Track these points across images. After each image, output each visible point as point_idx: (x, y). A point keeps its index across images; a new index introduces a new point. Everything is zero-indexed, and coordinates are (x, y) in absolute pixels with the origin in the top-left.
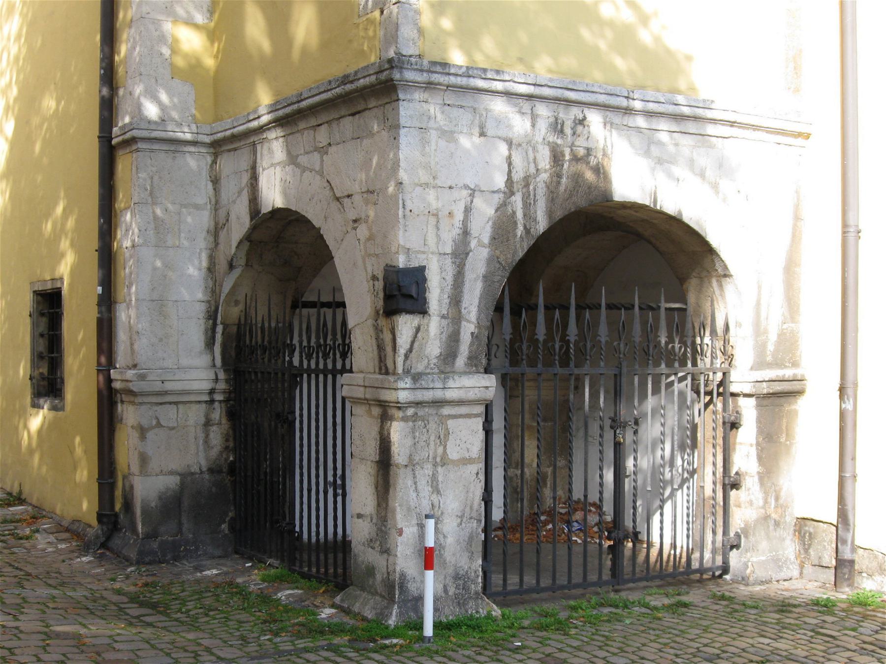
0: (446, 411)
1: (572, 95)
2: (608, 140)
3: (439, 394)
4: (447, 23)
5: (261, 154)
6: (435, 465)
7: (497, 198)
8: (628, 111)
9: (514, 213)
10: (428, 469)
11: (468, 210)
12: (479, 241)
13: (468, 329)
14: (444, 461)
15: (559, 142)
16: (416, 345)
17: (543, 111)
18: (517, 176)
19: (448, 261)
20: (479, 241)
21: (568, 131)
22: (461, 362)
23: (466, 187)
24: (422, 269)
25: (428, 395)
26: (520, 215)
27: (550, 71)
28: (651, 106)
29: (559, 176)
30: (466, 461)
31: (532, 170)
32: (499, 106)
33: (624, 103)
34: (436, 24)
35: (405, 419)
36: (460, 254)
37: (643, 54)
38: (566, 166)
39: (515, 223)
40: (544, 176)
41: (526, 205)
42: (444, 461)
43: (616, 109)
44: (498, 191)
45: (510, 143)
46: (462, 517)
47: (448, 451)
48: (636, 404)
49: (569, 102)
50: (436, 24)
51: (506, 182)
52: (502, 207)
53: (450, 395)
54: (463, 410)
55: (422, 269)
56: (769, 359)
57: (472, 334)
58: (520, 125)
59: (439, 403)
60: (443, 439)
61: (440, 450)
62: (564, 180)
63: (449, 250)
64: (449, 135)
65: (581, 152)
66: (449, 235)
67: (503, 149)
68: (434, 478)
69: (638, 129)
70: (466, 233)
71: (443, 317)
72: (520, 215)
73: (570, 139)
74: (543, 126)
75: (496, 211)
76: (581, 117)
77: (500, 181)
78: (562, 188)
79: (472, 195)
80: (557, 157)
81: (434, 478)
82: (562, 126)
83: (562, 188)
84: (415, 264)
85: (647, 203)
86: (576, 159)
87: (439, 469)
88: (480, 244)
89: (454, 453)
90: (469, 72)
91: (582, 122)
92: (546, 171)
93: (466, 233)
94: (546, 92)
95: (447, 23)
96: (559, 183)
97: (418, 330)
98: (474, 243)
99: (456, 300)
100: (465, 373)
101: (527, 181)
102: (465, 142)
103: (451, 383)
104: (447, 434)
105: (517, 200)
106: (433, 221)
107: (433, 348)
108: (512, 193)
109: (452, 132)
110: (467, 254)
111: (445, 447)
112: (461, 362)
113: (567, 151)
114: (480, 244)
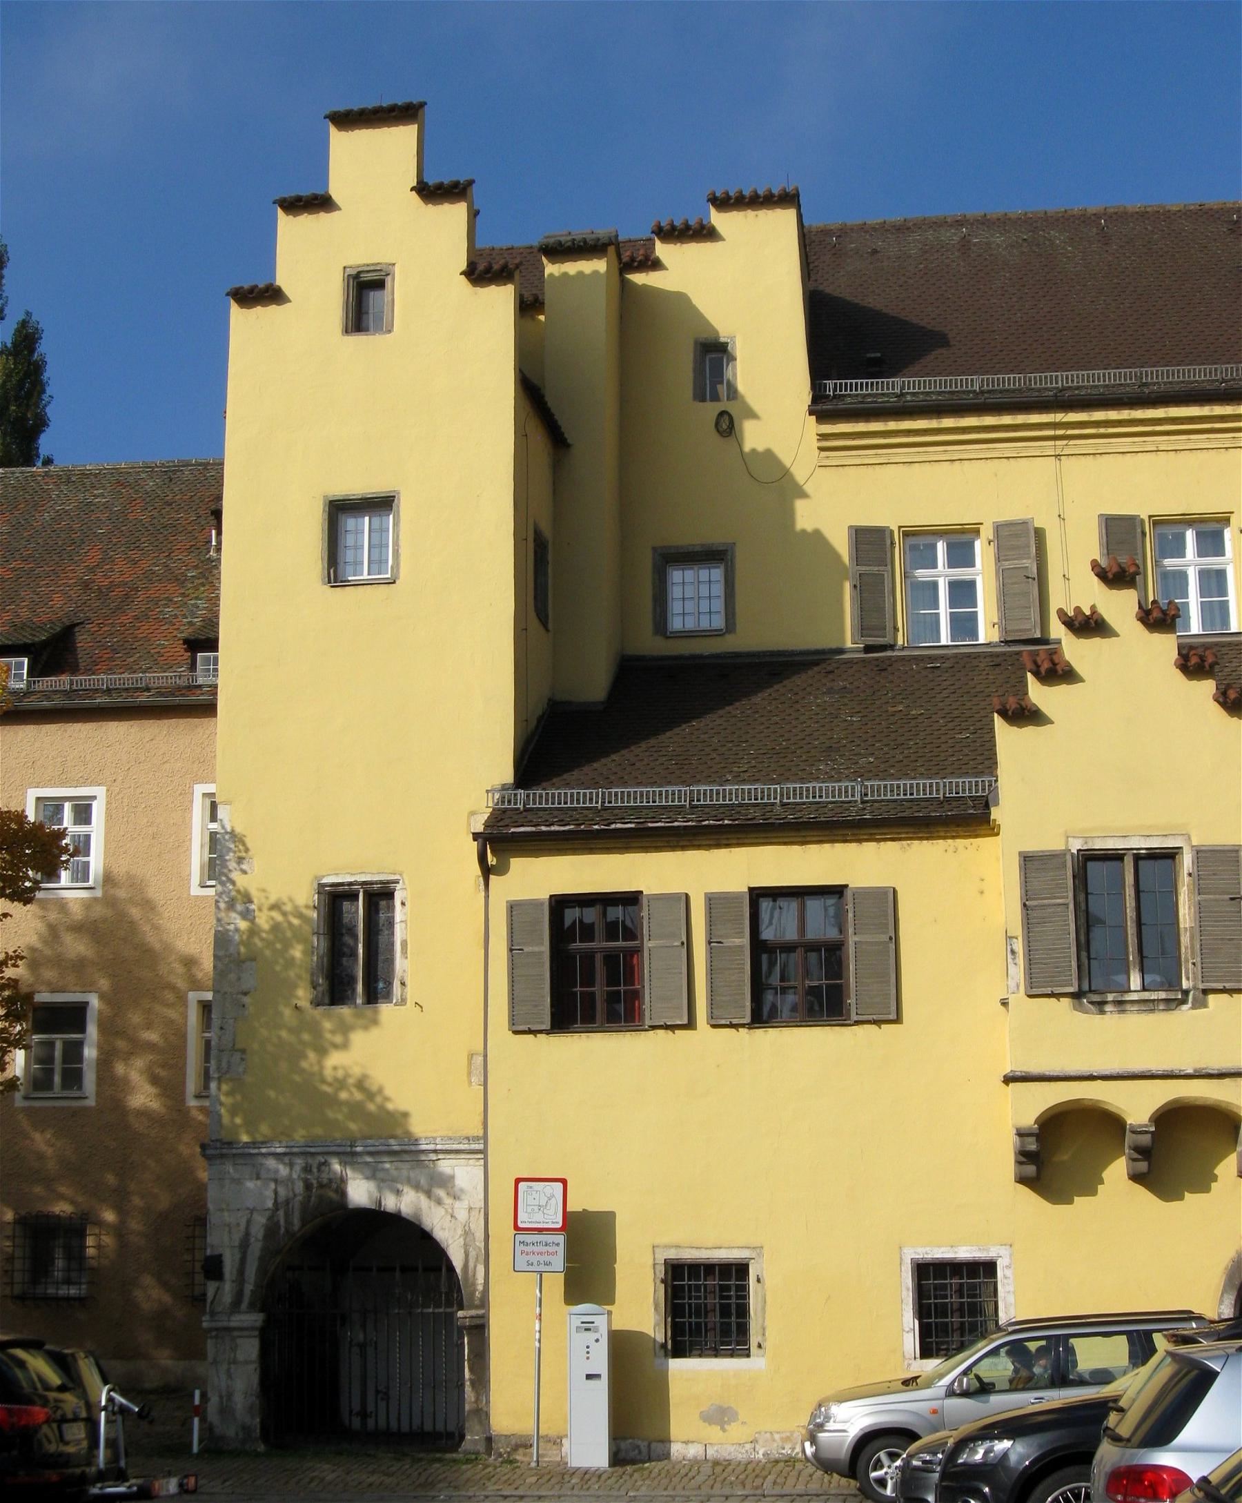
0: (236, 1333)
1: (312, 1150)
2: (344, 1172)
3: (225, 1324)
4: (238, 1121)
5: (469, 1159)
6: (229, 1364)
7: (268, 1214)
8: (354, 1154)
9: (278, 1221)
10: (225, 1366)
11: (249, 1222)
12: (256, 1238)
13: (249, 1288)
14: (235, 1362)
15: (309, 1177)
16: (217, 1297)
17: (299, 1162)
18: (280, 1200)
19: (236, 1251)
20: (256, 1238)
21: (315, 1170)
22: (244, 1306)
23: (248, 1209)
24: (220, 1256)
25: (220, 1324)
26: (282, 1222)
27: (304, 1137)
28: (371, 1149)
29: (310, 1197)
30: (247, 1362)
31: (291, 1195)
32: (271, 1163)
33: (349, 1149)
34: (232, 1122)
35: (211, 1338)
36: (244, 1245)
37: (367, 1117)
38: (314, 1190)
39: (280, 1227)
40: (300, 1198)
41: (287, 1215)
42: (235, 1362)
43: (344, 1153)
44: (269, 1209)
45: (276, 1181)
46: (246, 1393)
47: (238, 1356)
48: (78, 1471)
49: (313, 1154)
50: (232, 1122)
51: (273, 1204)
52: (270, 1218)
53: (232, 1324)
54: (246, 1333)
55: (220, 1256)
56: (477, 1302)
57: (252, 1291)
58: (283, 1171)
59: (228, 1329)
60: (234, 1349)
61: (232, 1355)
62: (313, 1198)
63: (237, 1244)
64: (238, 1182)
65: (325, 1181)
66: (237, 1237)
67: (272, 1186)
68: (228, 1371)
69: (367, 1163)
70: (247, 1234)
71: (233, 1281)
72: (282, 1222)
73: (316, 1174)
74: (297, 1168)
75: (268, 1220)
76: (323, 1160)
77: (270, 1204)
78: (311, 1204)
79: (252, 1214)
80: (308, 1186)
81: (228, 1371)
82: (311, 1167)
83: (311, 1204)
84: (216, 1253)
85: (373, 1208)
86: (321, 1186)
87: (232, 1366)
88: (257, 1240)
89: (240, 1357)
90: (254, 1144)
91: (326, 1163)
92: (301, 1195)
93: (247, 1234)
94: (295, 1150)
95: (238, 1121)
96: (309, 1201)
97: (218, 1289)
98: (252, 1240)
99: (241, 1271)
100: (247, 1312)
101: (287, 1202)
102: (250, 1185)
103: (233, 1318)
104: (236, 1346)
105: (281, 1213)
106: (227, 1229)
107: (227, 1298)
108: (277, 1210)
109: (239, 1179)
110: (248, 1246)
111: (235, 1354)
112: (244, 1306)
113: (315, 1182)
114: (257, 1240)
